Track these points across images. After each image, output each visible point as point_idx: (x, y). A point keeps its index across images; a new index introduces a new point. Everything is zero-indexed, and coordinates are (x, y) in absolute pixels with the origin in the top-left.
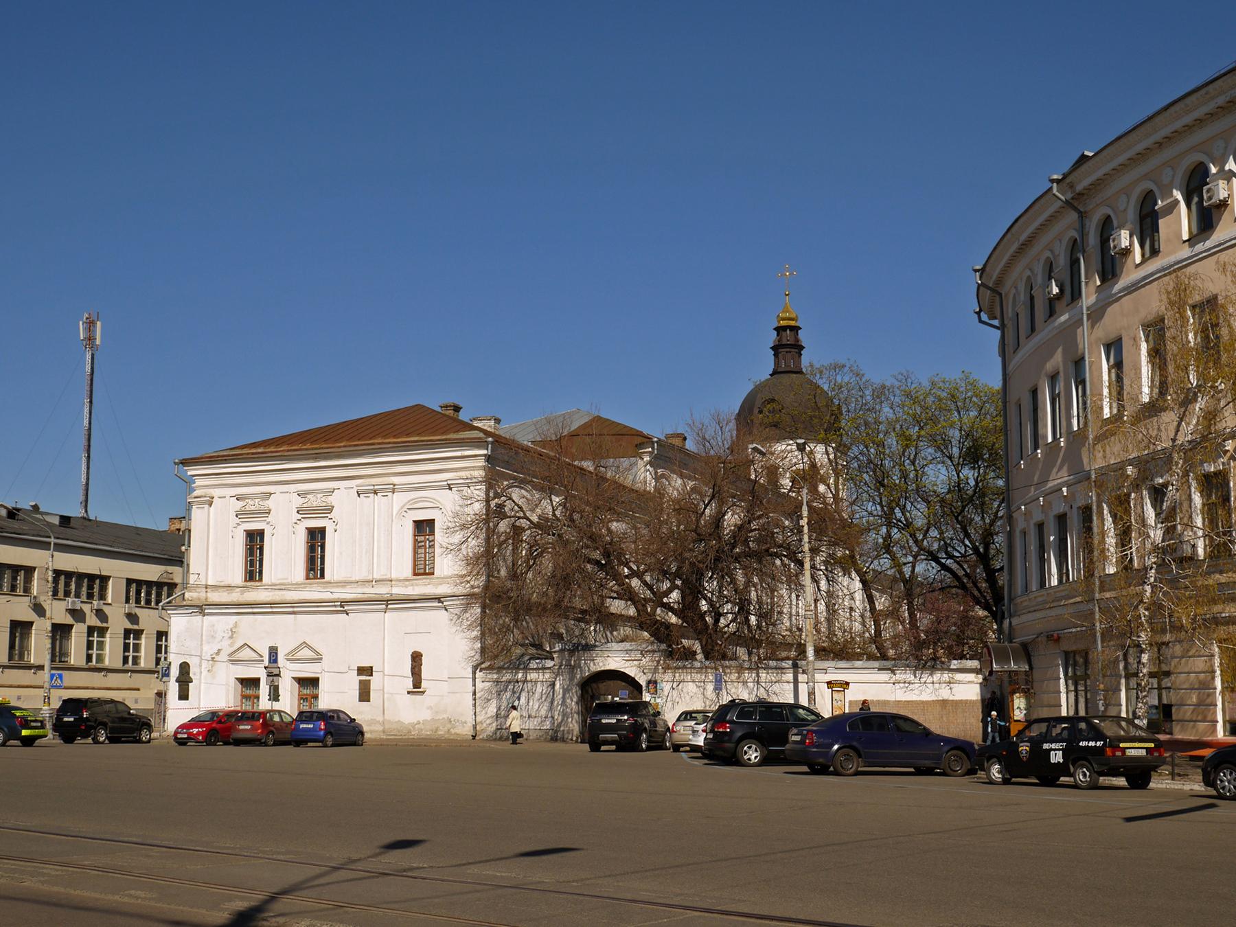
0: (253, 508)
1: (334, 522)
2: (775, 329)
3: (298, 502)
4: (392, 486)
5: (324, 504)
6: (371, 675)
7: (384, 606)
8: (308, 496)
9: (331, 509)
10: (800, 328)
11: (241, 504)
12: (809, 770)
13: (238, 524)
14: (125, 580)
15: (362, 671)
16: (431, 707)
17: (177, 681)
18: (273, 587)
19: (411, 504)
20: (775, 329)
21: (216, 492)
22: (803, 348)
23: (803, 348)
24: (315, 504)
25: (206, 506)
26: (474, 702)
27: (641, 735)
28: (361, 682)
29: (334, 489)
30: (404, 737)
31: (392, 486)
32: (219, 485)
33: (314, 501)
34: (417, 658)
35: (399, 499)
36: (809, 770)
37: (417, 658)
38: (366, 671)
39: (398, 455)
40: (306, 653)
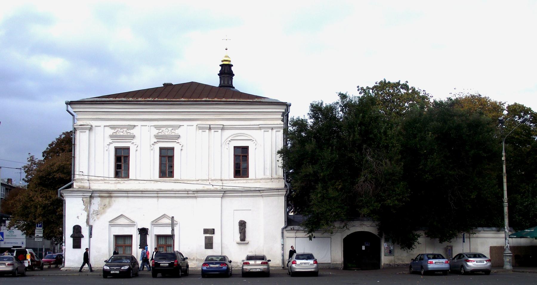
0: (122, 134)
1: (180, 144)
2: (220, 65)
3: (155, 132)
4: (222, 126)
5: (173, 134)
6: (214, 233)
7: (222, 195)
8: (162, 129)
9: (178, 137)
10: (232, 66)
11: (113, 131)
12: (511, 252)
13: (111, 143)
14: (131, 177)
15: (206, 231)
16: (252, 251)
17: (71, 237)
18: (256, 180)
19: (233, 137)
20: (220, 65)
21: (94, 123)
22: (234, 75)
23: (234, 75)
24: (167, 134)
25: (207, 131)
26: (282, 246)
27: (131, 271)
28: (206, 238)
29: (180, 126)
30: (236, 269)
31: (222, 126)
32: (91, 119)
33: (167, 132)
34: (242, 225)
35: (227, 133)
36: (511, 252)
37: (242, 225)
38: (210, 231)
39: (154, 108)
40: (122, 221)
